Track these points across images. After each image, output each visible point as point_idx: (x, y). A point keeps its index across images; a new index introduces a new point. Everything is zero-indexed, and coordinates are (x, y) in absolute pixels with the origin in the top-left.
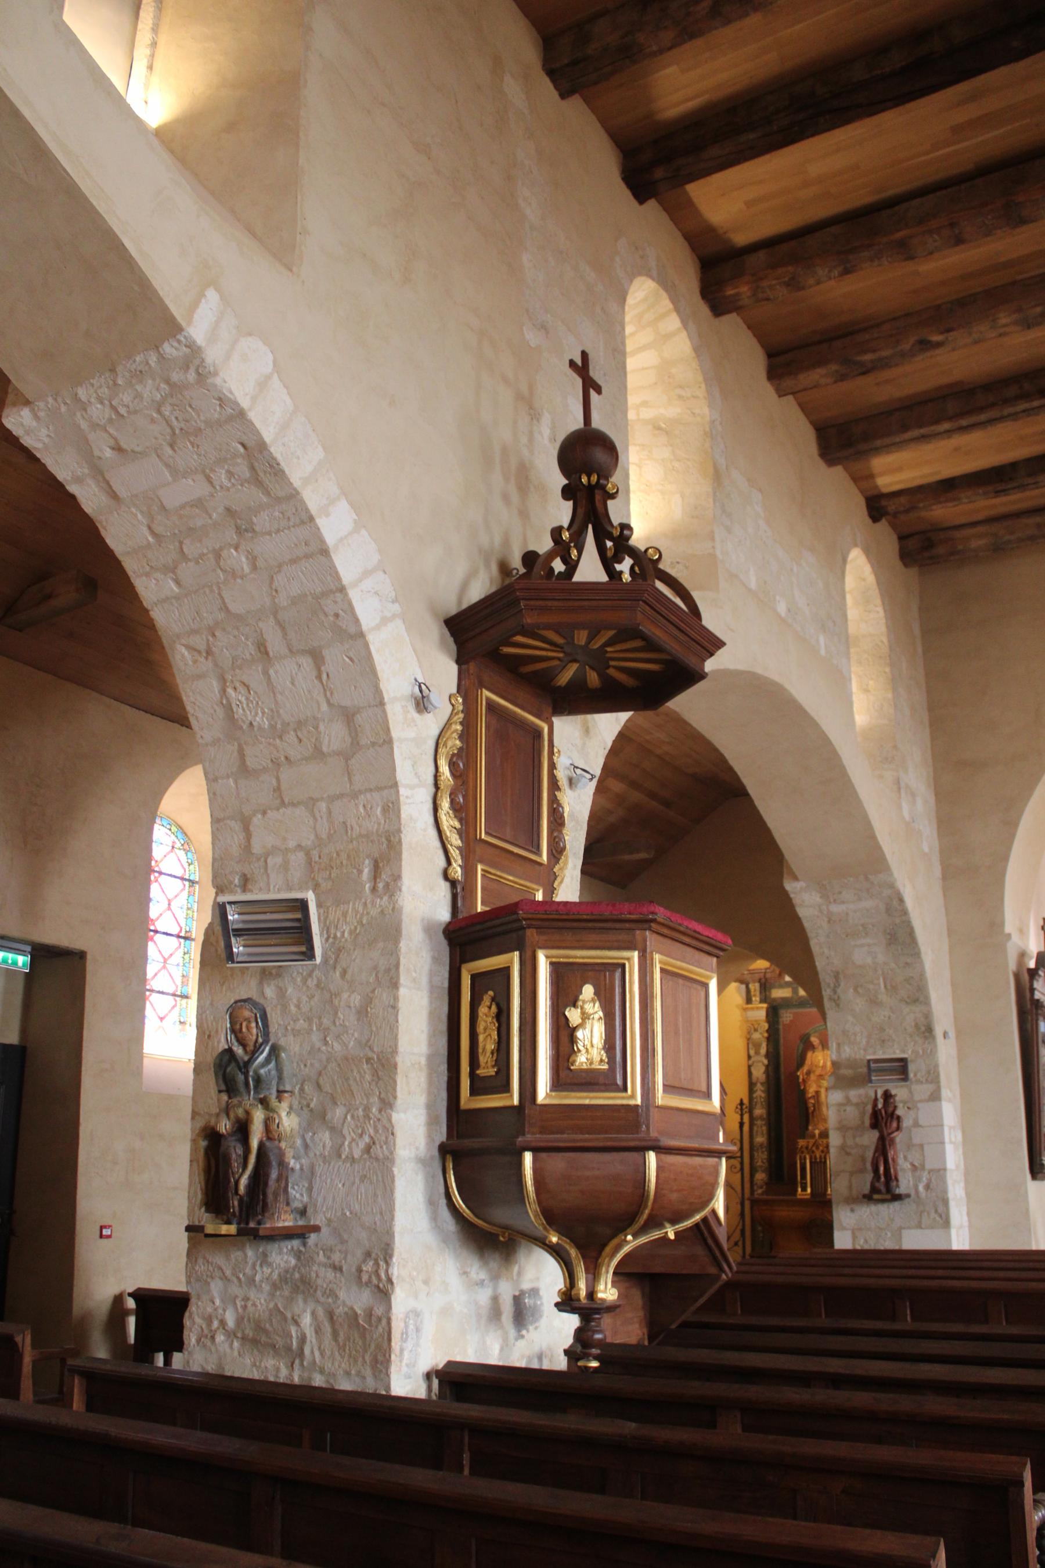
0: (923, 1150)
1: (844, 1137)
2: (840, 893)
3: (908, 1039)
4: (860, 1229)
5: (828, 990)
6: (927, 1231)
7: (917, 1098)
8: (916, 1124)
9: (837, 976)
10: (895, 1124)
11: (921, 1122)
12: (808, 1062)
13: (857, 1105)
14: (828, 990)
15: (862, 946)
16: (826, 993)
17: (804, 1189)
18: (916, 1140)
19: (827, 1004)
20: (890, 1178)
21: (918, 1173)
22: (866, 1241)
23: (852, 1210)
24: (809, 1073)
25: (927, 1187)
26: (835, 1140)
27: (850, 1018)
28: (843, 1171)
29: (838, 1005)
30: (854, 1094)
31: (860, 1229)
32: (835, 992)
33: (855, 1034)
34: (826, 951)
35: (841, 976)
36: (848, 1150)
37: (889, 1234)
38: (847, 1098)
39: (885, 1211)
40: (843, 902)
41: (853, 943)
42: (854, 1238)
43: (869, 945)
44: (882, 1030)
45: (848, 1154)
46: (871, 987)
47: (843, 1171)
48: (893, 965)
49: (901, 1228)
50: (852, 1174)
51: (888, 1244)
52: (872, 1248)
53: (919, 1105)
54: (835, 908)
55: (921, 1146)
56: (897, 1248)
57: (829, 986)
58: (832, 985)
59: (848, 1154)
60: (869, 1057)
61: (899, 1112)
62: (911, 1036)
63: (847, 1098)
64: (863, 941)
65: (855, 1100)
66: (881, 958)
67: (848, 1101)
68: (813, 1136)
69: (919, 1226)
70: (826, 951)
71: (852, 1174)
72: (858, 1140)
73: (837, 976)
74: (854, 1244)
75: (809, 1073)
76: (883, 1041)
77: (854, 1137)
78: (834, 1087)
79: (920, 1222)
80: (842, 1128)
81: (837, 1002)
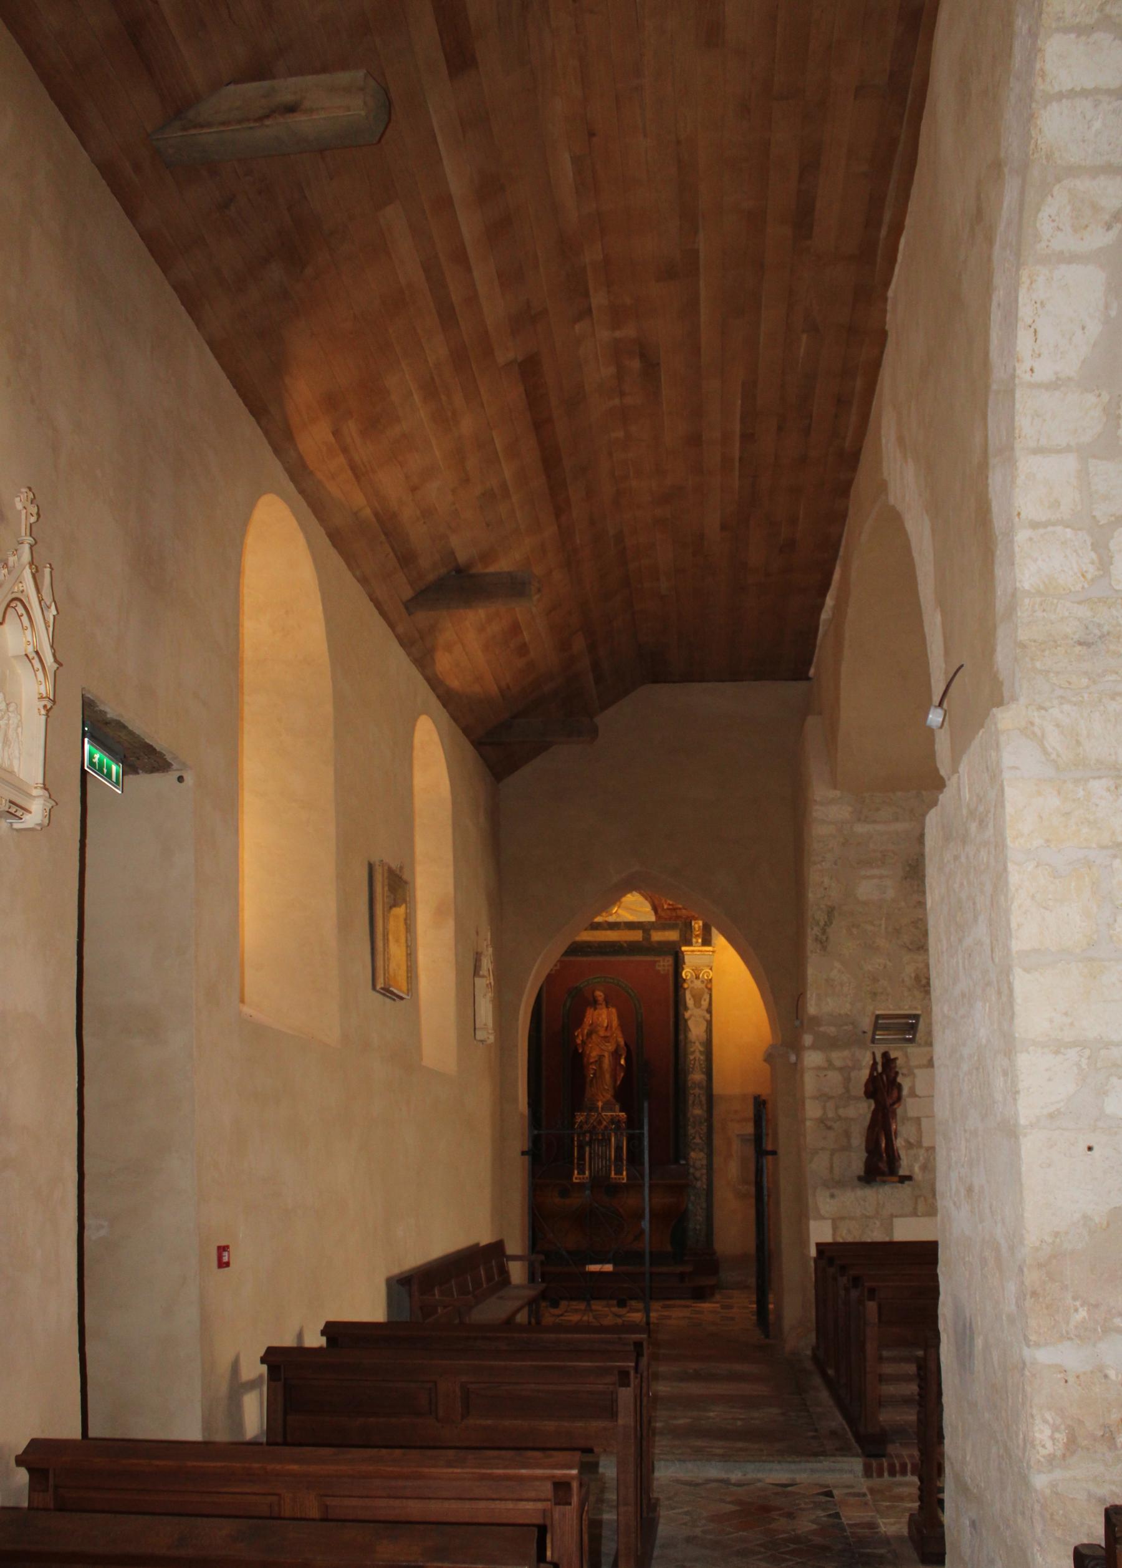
0: (920, 1124)
1: (824, 1108)
2: (878, 810)
3: (906, 994)
4: (842, 1218)
5: (816, 929)
6: (922, 1219)
7: (913, 1063)
8: (913, 1094)
9: (830, 911)
10: (895, 1094)
11: (918, 1092)
12: (588, 1020)
13: (841, 1069)
14: (816, 929)
15: (872, 877)
16: (812, 932)
17: (582, 1171)
18: (912, 1113)
19: (810, 944)
20: (893, 1159)
21: (912, 1152)
22: (849, 1231)
23: (832, 1196)
24: (590, 1034)
25: (924, 1168)
26: (812, 1110)
27: (837, 964)
28: (823, 1149)
29: (824, 948)
30: (839, 1057)
31: (842, 1218)
32: (824, 932)
33: (842, 985)
34: (826, 880)
35: (836, 914)
36: (829, 1123)
37: (878, 1223)
38: (829, 1062)
39: (884, 1195)
40: (875, 822)
41: (863, 873)
42: (835, 1229)
43: (881, 877)
44: (875, 980)
45: (830, 1128)
46: (869, 928)
47: (823, 1149)
48: (903, 904)
49: (892, 1216)
50: (833, 1152)
51: (876, 1235)
52: (857, 1240)
53: (916, 1071)
54: (861, 829)
55: (918, 1119)
56: (887, 1239)
57: (818, 924)
58: (822, 923)
59: (830, 1128)
60: (878, 1012)
61: (899, 1079)
62: (909, 990)
63: (829, 1062)
64: (876, 872)
65: (838, 1063)
66: (890, 894)
67: (830, 1065)
68: (593, 1108)
69: (915, 1214)
70: (826, 880)
71: (833, 1152)
72: (841, 1111)
73: (830, 911)
74: (834, 1235)
75: (590, 1034)
76: (875, 994)
77: (837, 1108)
78: (814, 1047)
79: (915, 1208)
80: (823, 1097)
81: (823, 943)
